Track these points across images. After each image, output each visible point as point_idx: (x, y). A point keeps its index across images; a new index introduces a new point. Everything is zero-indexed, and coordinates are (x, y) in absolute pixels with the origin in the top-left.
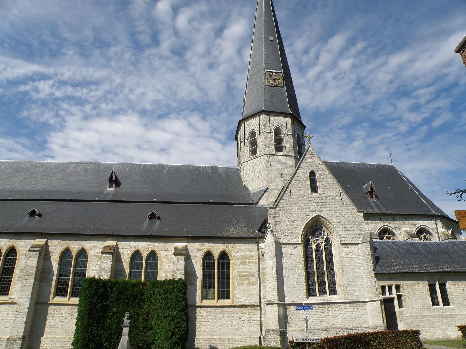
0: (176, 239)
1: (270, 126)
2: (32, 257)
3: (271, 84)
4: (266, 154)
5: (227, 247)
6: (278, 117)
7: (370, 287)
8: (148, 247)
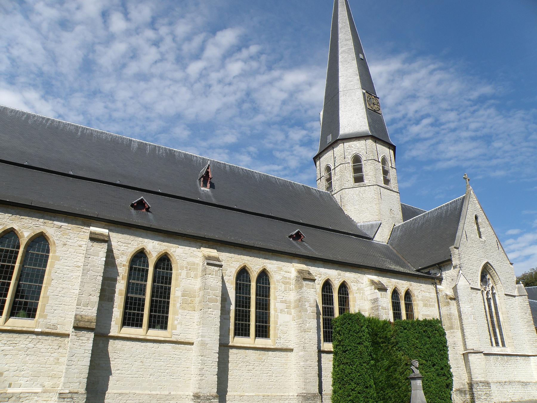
0: (365, 269)
1: (378, 154)
2: (213, 275)
3: (371, 108)
4: (377, 185)
5: (411, 285)
6: (383, 147)
8: (339, 277)
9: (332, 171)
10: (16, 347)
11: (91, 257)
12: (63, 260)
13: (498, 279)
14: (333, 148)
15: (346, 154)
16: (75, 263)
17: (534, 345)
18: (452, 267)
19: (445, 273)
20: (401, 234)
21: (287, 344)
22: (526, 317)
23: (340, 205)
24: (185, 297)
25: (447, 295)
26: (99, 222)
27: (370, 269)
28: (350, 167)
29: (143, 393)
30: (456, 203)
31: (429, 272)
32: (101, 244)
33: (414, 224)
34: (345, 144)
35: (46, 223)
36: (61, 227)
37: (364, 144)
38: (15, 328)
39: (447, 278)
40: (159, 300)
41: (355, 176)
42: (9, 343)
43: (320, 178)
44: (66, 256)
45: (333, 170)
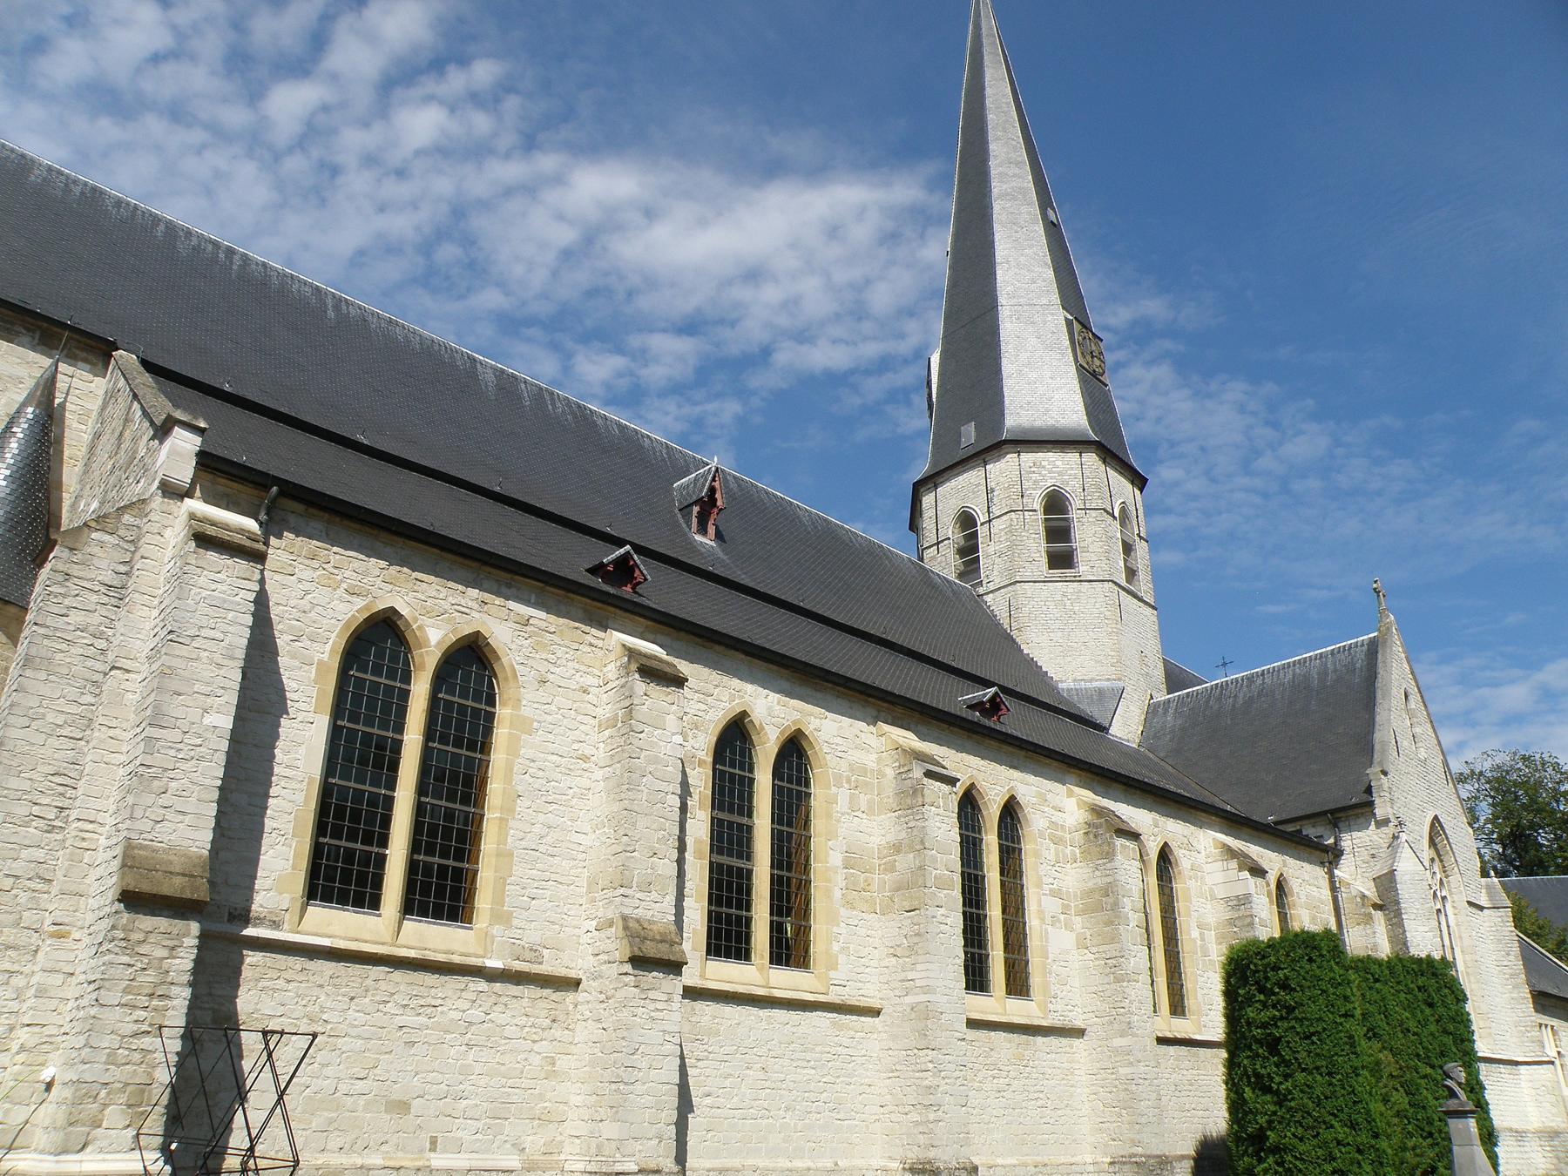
4: (1111, 581)
6: (1119, 477)
7: (1525, 1024)
9: (978, 528)
10: (436, 1019)
11: (646, 730)
12: (540, 732)
13: (1454, 861)
14: (985, 463)
15: (1026, 484)
16: (576, 746)
17: (1529, 1035)
18: (1373, 823)
19: (1350, 837)
20: (1179, 722)
21: (1071, 1014)
22: (1509, 963)
23: (1006, 626)
24: (852, 871)
25: (1364, 896)
26: (632, 616)
27: (1212, 814)
28: (1036, 524)
29: (775, 1165)
30: (1350, 654)
31: (1300, 831)
32: (668, 690)
33: (1219, 699)
34: (1023, 456)
35: (486, 603)
36: (528, 620)
37: (1076, 464)
38: (432, 956)
39: (1358, 852)
40: (453, 867)
41: (1051, 549)
42: (413, 1003)
43: (938, 543)
44: (549, 719)
45: (982, 524)
